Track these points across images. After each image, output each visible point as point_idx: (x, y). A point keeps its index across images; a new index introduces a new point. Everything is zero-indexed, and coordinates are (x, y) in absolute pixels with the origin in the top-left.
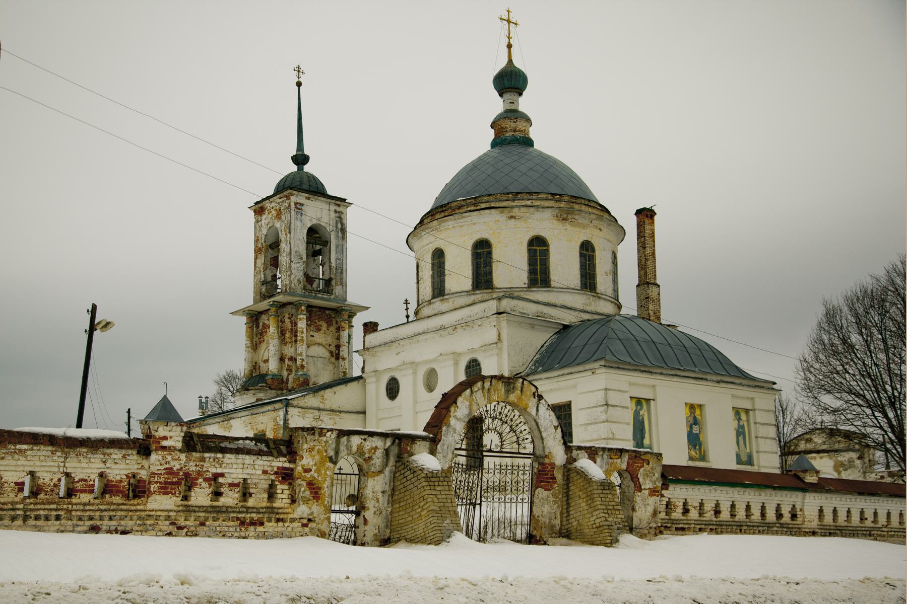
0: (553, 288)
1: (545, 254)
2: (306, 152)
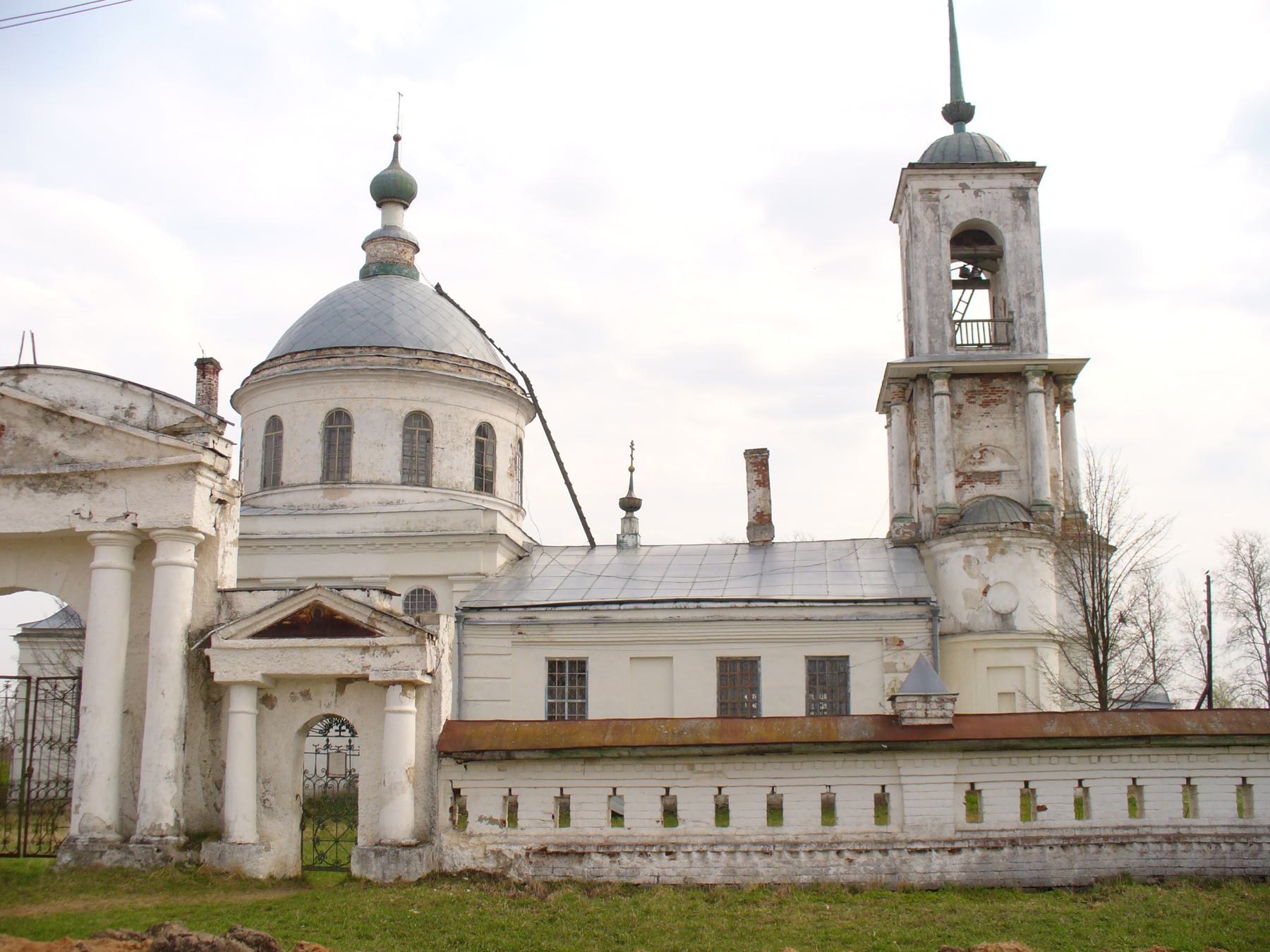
0: (354, 483)
1: (347, 432)
2: (968, 98)
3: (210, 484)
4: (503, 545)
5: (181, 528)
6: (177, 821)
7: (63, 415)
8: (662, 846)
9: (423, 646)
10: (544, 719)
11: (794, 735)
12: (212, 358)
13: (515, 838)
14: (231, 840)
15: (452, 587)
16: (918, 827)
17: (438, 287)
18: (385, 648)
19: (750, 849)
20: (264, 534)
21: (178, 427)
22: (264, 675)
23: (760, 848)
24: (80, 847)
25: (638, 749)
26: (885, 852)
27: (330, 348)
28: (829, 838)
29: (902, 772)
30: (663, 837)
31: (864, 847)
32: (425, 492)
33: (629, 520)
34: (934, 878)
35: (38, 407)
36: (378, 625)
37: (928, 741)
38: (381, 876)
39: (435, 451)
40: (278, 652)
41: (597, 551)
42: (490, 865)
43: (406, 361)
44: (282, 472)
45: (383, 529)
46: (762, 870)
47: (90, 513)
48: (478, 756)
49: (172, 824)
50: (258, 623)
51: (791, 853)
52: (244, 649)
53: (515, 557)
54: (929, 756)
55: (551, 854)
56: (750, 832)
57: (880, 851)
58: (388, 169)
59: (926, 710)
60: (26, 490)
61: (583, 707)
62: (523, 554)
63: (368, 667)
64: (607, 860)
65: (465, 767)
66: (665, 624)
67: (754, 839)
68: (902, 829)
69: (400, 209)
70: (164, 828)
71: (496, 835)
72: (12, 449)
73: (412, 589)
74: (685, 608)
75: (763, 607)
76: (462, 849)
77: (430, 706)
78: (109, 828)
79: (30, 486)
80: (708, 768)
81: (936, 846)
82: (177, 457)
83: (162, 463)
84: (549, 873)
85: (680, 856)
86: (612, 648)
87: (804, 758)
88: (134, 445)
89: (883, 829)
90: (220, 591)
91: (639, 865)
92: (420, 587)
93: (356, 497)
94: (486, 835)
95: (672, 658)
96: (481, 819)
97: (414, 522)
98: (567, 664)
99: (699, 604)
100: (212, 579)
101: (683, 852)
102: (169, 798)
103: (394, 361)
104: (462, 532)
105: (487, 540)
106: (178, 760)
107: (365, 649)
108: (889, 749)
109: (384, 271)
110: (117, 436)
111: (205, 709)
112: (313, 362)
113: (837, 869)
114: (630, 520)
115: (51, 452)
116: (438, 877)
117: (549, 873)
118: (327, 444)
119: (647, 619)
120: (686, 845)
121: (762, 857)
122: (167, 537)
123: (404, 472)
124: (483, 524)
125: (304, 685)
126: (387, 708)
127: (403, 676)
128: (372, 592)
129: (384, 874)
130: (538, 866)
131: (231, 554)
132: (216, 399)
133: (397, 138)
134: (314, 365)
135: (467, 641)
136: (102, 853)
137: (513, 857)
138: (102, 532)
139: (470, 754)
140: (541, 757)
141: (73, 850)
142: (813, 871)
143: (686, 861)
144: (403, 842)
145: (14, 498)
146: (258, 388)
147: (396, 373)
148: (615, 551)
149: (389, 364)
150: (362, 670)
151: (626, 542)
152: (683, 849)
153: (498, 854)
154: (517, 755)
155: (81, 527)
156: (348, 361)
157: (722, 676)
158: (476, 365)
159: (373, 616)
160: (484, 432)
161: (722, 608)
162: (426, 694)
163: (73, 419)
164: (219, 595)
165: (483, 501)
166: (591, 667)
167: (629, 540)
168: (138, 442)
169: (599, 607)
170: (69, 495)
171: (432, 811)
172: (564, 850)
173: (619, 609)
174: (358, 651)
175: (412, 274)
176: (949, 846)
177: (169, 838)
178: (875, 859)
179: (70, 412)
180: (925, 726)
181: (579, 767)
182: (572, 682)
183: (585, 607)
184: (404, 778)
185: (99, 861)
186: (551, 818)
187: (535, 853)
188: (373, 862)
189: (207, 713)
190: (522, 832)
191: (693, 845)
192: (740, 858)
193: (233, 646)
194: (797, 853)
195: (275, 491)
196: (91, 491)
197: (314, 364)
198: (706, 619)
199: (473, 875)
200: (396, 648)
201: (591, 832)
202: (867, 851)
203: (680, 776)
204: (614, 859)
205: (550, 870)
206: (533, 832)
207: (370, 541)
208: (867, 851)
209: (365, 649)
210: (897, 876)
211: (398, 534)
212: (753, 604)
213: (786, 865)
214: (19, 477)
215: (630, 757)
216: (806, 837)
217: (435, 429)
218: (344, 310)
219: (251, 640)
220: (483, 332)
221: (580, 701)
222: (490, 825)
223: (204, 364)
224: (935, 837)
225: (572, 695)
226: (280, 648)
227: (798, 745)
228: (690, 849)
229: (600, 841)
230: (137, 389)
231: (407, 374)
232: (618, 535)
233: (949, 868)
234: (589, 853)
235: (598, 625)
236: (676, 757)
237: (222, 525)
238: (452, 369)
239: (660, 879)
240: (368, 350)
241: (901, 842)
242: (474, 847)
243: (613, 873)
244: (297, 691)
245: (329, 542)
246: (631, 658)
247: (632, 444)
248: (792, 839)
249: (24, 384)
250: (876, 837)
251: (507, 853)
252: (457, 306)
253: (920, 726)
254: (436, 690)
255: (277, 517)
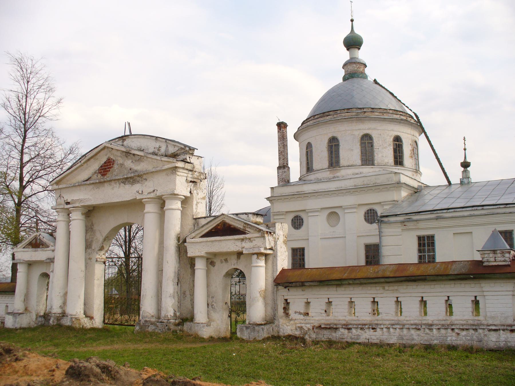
0: (342, 167)
1: (337, 146)
3: (186, 175)
4: (404, 187)
5: (171, 194)
6: (175, 314)
7: (131, 153)
8: (370, 325)
9: (264, 237)
10: (291, 268)
11: (429, 272)
12: (283, 122)
13: (309, 321)
14: (195, 322)
15: (383, 207)
16: (492, 318)
17: (375, 81)
18: (250, 239)
19: (410, 327)
20: (306, 191)
21: (176, 153)
22: (206, 253)
23: (414, 327)
24: (142, 324)
25: (357, 280)
26: (476, 330)
27: (328, 112)
28: (448, 322)
29: (484, 289)
30: (372, 321)
31: (465, 327)
32: (372, 168)
33: (465, 172)
34: (502, 344)
35: (123, 152)
36: (247, 229)
37: (494, 274)
38: (248, 338)
39: (375, 150)
40: (210, 243)
41: (453, 187)
42: (297, 333)
43: (359, 113)
44: (313, 165)
45: (353, 185)
46: (415, 337)
47: (142, 191)
48: (290, 285)
49: (172, 315)
50: (202, 231)
51: (430, 329)
52: (198, 242)
53: (413, 192)
54: (498, 281)
55: (324, 328)
56: (411, 319)
57: (473, 329)
58: (349, 34)
59: (495, 257)
60: (122, 184)
61: (434, 258)
62: (417, 191)
63: (244, 247)
64: (346, 331)
65: (288, 289)
66: (467, 217)
67: (412, 322)
68: (485, 319)
69: (357, 50)
70: (169, 316)
71: (302, 319)
72: (117, 169)
73: (367, 210)
74: (476, 210)
75: (513, 207)
76: (287, 326)
77: (273, 263)
78: (153, 316)
79: (122, 183)
80: (391, 288)
81: (502, 328)
82: (168, 166)
83: (163, 168)
84: (322, 337)
85: (378, 330)
86: (445, 229)
87: (435, 283)
88: (154, 162)
89: (477, 318)
90: (194, 219)
91: (360, 334)
92: (370, 208)
93: (342, 173)
94: (298, 319)
95: (472, 232)
96: (296, 312)
97: (366, 181)
98: (426, 238)
99: (483, 207)
100: (191, 214)
101: (379, 328)
102: (171, 305)
103: (354, 114)
104: (386, 183)
105: (396, 186)
106: (174, 289)
107: (243, 240)
108: (474, 278)
109: (351, 77)
110: (149, 159)
111: (190, 268)
112: (321, 118)
113: (451, 338)
114: (466, 172)
115: (129, 169)
116: (275, 338)
117: (322, 337)
118: (330, 152)
119: (460, 216)
120: (381, 325)
121: (416, 331)
122: (168, 198)
123: (362, 160)
124: (395, 179)
125: (225, 256)
126: (252, 265)
127: (256, 251)
128: (249, 215)
129: (249, 337)
130: (317, 334)
131: (201, 203)
132: (287, 138)
133: (352, 21)
134: (322, 120)
135: (383, 230)
136: (149, 326)
137: (307, 329)
138: (145, 198)
139: (287, 284)
140: (316, 284)
141: (139, 325)
142: (440, 339)
143: (381, 332)
144: (258, 323)
145: (118, 188)
146: (302, 132)
147: (355, 119)
148: (460, 185)
149: (352, 116)
150: (242, 249)
151: (465, 181)
152: (379, 327)
153: (301, 328)
154: (306, 284)
155: (139, 197)
156: (335, 116)
157: (300, 249)
158: (391, 112)
159: (245, 225)
160: (398, 140)
161: (493, 208)
162: (271, 258)
163: (134, 155)
164: (194, 221)
165: (398, 169)
166: (436, 238)
167: (466, 181)
168: (155, 161)
169: (438, 212)
170: (135, 184)
171: (275, 309)
172: (328, 327)
173: (447, 212)
174: (240, 241)
175: (365, 77)
176: (509, 328)
177: (171, 321)
178: (470, 334)
179: (132, 152)
180: (495, 266)
181: (335, 289)
182: (429, 246)
183: (432, 212)
184: (258, 295)
185: (147, 329)
186: (324, 312)
187: (317, 328)
188: (245, 332)
189: (191, 269)
190: (311, 318)
191: (384, 325)
192: (405, 331)
193: (194, 241)
194: (432, 329)
195: (311, 173)
196: (142, 182)
197: (321, 119)
198: (486, 214)
199: (291, 338)
200: (254, 239)
201: (341, 318)
202: (467, 329)
203: (379, 292)
204: (350, 331)
205: (322, 336)
206: (317, 318)
207: (348, 191)
208: (467, 329)
209: (243, 240)
210: (482, 342)
211: (360, 187)
212: (508, 206)
213: (427, 335)
214: (118, 180)
215: (353, 284)
216: (437, 322)
217: (374, 140)
218: (334, 95)
219: (200, 239)
220: (396, 97)
221: (432, 254)
222: (299, 315)
223: (280, 125)
224: (503, 323)
225: (429, 251)
226: (211, 241)
227: (429, 277)
228: (382, 327)
229: (344, 322)
230: (161, 139)
231: (360, 119)
232: (460, 179)
233: (510, 340)
234: (339, 328)
235: (438, 220)
236: (376, 283)
237: (195, 191)
238: (380, 114)
239: (369, 340)
240: (343, 110)
241: (484, 325)
242: (292, 324)
243: (349, 337)
244: (223, 259)
245: (332, 192)
246: (454, 234)
247: (464, 138)
248: (430, 322)
249: (125, 143)
250: (471, 322)
251: (305, 328)
252: (384, 88)
253: (492, 266)
254: (275, 256)
255: (311, 184)
